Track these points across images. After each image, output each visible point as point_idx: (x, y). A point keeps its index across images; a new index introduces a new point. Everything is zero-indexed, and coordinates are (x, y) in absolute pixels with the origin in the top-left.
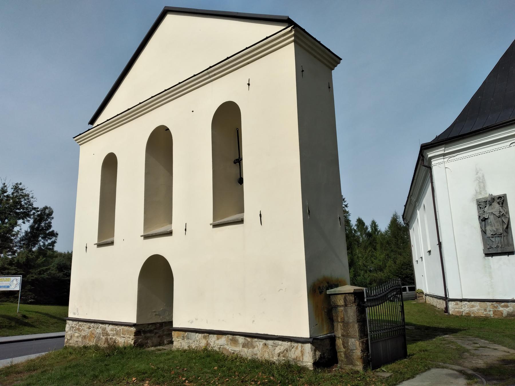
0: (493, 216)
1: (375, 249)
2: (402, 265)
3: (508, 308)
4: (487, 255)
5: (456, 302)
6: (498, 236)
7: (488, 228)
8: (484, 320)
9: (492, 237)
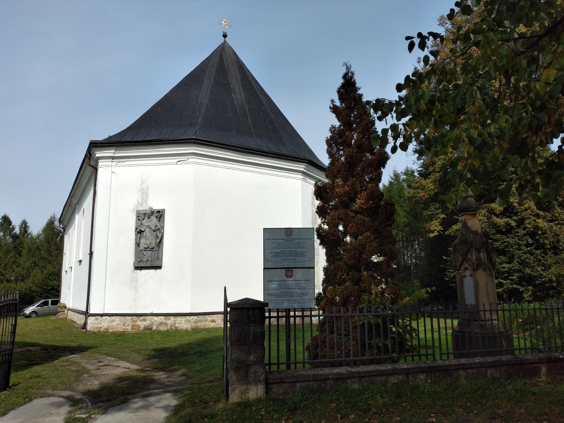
0: (149, 230)
1: (20, 255)
2: (50, 275)
3: (146, 322)
4: (137, 268)
5: (96, 317)
6: (150, 249)
7: (143, 241)
8: (120, 336)
9: (144, 250)
